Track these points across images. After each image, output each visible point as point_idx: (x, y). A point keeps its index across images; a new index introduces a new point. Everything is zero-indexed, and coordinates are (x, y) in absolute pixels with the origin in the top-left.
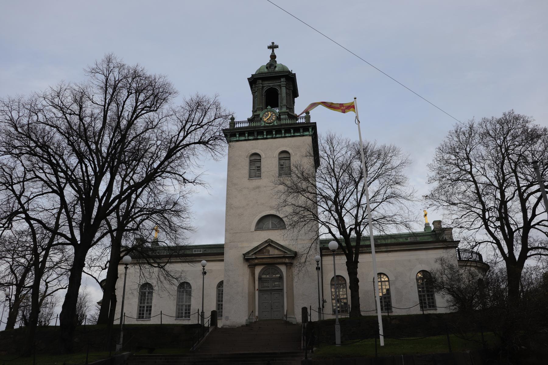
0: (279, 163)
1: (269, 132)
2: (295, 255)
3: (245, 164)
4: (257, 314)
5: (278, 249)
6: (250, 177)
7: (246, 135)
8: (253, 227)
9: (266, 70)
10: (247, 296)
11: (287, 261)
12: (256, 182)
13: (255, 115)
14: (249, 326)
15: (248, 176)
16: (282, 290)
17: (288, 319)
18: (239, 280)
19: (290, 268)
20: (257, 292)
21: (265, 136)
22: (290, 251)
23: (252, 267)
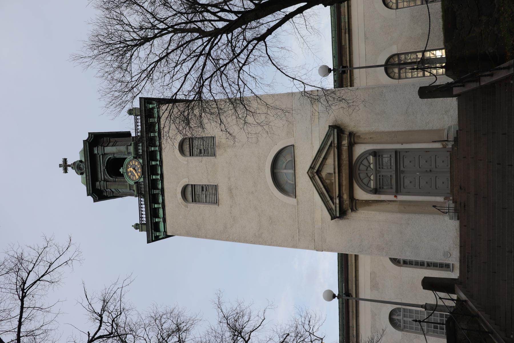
0: (197, 156)
1: (153, 170)
2: (337, 130)
3: (201, 210)
4: (440, 199)
5: (325, 158)
6: (216, 202)
7: (156, 206)
8: (291, 201)
9: (84, 175)
10: (406, 216)
11: (345, 142)
12: (223, 194)
13: (138, 193)
14: (461, 212)
15: (213, 206)
16: (397, 152)
17: (451, 138)
18: (375, 226)
19: (359, 136)
20: (400, 198)
21: (159, 177)
22: (328, 136)
23: (355, 204)
